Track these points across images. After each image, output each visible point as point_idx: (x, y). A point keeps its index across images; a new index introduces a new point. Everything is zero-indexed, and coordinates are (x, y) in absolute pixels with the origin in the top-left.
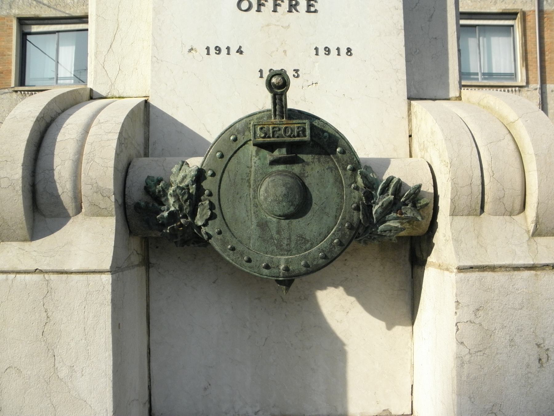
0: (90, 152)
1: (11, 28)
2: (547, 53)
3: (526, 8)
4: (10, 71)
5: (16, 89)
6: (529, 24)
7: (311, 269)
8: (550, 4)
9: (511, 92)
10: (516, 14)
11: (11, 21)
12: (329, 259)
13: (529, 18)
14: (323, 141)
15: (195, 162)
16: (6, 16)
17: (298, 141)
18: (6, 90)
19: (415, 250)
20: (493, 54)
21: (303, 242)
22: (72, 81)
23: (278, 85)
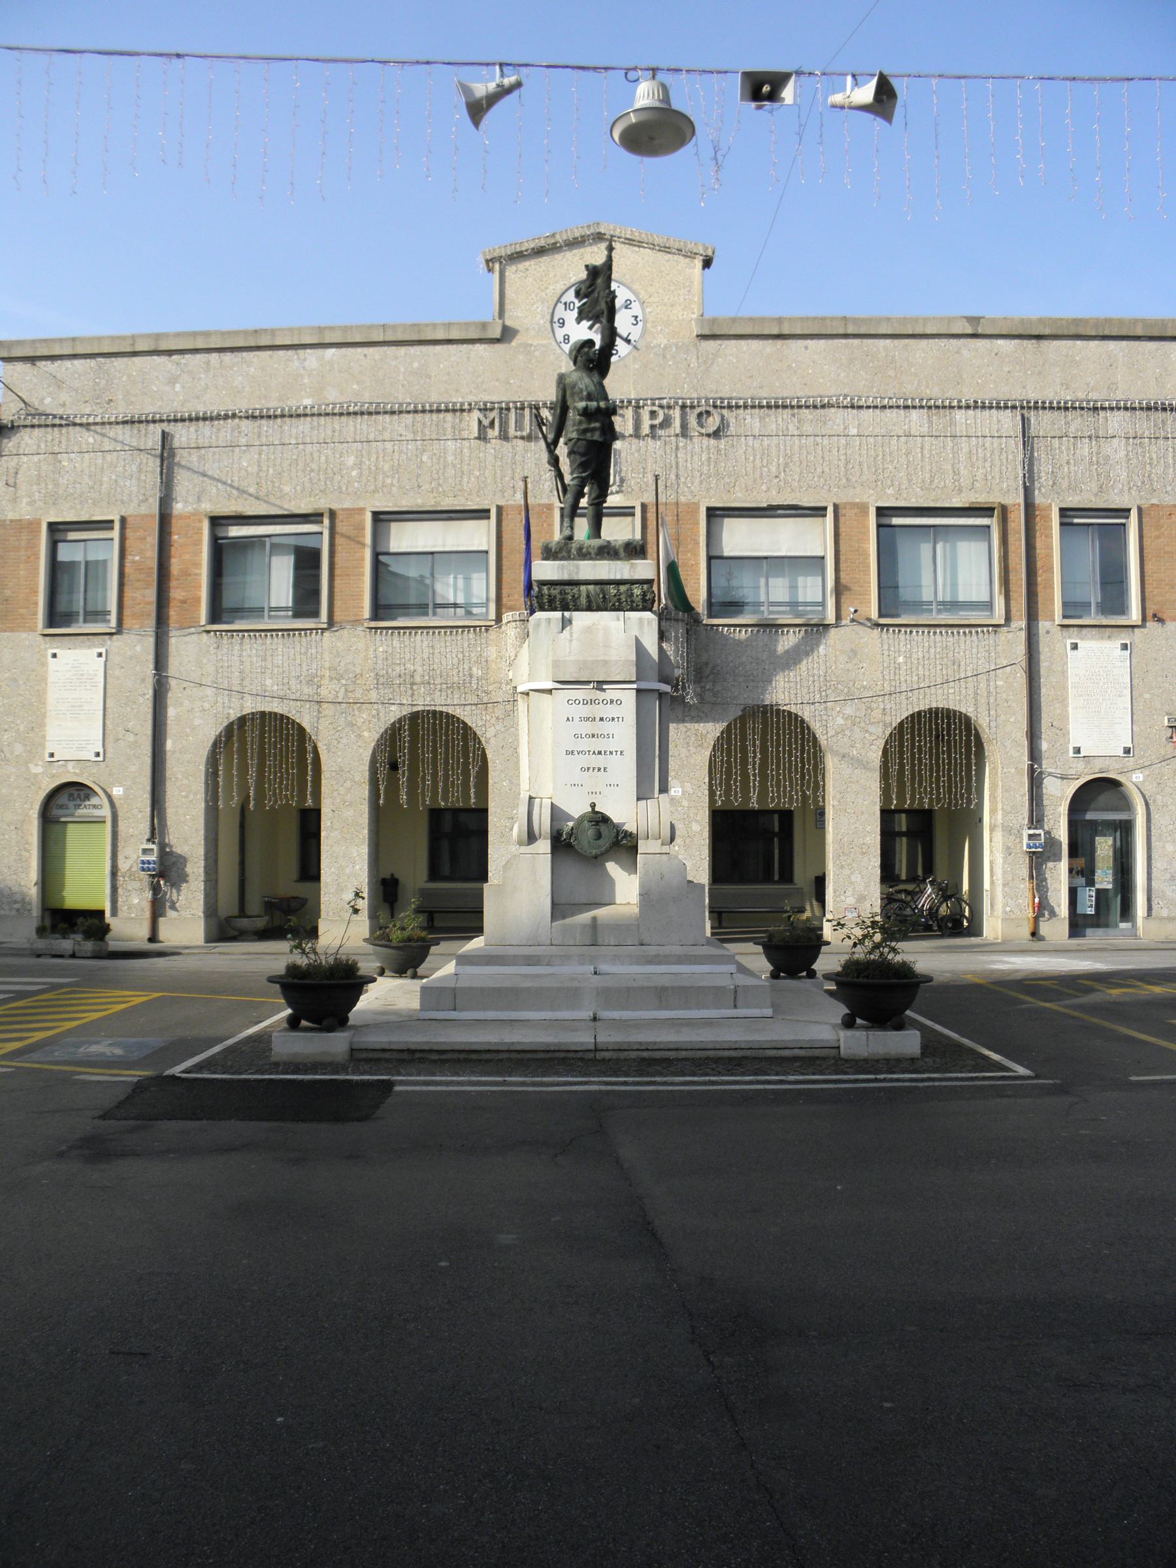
0: (543, 822)
1: (199, 531)
2: (1040, 572)
3: (1007, 501)
4: (198, 600)
5: (209, 627)
6: (1011, 525)
7: (602, 854)
8: (1044, 495)
9: (981, 635)
10: (992, 509)
11: (201, 521)
12: (607, 851)
13: (1012, 516)
14: (605, 820)
15: (571, 824)
16: (193, 514)
17: (599, 820)
18: (193, 630)
19: (634, 849)
20: (959, 569)
21: (600, 846)
22: (290, 613)
23: (593, 805)
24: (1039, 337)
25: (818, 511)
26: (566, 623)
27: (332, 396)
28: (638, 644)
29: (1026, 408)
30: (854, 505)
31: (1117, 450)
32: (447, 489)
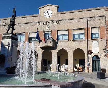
24: (89, 10)
25: (67, 30)
26: (4, 40)
27: (26, 22)
28: (9, 42)
29: (87, 18)
30: (70, 29)
31: (97, 21)
32: (96, 21)
